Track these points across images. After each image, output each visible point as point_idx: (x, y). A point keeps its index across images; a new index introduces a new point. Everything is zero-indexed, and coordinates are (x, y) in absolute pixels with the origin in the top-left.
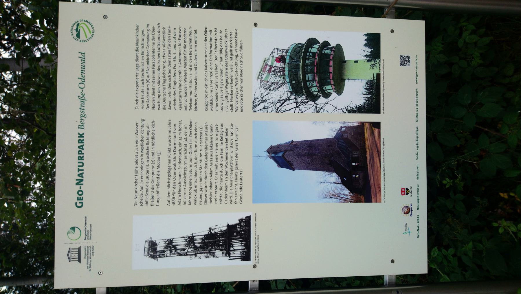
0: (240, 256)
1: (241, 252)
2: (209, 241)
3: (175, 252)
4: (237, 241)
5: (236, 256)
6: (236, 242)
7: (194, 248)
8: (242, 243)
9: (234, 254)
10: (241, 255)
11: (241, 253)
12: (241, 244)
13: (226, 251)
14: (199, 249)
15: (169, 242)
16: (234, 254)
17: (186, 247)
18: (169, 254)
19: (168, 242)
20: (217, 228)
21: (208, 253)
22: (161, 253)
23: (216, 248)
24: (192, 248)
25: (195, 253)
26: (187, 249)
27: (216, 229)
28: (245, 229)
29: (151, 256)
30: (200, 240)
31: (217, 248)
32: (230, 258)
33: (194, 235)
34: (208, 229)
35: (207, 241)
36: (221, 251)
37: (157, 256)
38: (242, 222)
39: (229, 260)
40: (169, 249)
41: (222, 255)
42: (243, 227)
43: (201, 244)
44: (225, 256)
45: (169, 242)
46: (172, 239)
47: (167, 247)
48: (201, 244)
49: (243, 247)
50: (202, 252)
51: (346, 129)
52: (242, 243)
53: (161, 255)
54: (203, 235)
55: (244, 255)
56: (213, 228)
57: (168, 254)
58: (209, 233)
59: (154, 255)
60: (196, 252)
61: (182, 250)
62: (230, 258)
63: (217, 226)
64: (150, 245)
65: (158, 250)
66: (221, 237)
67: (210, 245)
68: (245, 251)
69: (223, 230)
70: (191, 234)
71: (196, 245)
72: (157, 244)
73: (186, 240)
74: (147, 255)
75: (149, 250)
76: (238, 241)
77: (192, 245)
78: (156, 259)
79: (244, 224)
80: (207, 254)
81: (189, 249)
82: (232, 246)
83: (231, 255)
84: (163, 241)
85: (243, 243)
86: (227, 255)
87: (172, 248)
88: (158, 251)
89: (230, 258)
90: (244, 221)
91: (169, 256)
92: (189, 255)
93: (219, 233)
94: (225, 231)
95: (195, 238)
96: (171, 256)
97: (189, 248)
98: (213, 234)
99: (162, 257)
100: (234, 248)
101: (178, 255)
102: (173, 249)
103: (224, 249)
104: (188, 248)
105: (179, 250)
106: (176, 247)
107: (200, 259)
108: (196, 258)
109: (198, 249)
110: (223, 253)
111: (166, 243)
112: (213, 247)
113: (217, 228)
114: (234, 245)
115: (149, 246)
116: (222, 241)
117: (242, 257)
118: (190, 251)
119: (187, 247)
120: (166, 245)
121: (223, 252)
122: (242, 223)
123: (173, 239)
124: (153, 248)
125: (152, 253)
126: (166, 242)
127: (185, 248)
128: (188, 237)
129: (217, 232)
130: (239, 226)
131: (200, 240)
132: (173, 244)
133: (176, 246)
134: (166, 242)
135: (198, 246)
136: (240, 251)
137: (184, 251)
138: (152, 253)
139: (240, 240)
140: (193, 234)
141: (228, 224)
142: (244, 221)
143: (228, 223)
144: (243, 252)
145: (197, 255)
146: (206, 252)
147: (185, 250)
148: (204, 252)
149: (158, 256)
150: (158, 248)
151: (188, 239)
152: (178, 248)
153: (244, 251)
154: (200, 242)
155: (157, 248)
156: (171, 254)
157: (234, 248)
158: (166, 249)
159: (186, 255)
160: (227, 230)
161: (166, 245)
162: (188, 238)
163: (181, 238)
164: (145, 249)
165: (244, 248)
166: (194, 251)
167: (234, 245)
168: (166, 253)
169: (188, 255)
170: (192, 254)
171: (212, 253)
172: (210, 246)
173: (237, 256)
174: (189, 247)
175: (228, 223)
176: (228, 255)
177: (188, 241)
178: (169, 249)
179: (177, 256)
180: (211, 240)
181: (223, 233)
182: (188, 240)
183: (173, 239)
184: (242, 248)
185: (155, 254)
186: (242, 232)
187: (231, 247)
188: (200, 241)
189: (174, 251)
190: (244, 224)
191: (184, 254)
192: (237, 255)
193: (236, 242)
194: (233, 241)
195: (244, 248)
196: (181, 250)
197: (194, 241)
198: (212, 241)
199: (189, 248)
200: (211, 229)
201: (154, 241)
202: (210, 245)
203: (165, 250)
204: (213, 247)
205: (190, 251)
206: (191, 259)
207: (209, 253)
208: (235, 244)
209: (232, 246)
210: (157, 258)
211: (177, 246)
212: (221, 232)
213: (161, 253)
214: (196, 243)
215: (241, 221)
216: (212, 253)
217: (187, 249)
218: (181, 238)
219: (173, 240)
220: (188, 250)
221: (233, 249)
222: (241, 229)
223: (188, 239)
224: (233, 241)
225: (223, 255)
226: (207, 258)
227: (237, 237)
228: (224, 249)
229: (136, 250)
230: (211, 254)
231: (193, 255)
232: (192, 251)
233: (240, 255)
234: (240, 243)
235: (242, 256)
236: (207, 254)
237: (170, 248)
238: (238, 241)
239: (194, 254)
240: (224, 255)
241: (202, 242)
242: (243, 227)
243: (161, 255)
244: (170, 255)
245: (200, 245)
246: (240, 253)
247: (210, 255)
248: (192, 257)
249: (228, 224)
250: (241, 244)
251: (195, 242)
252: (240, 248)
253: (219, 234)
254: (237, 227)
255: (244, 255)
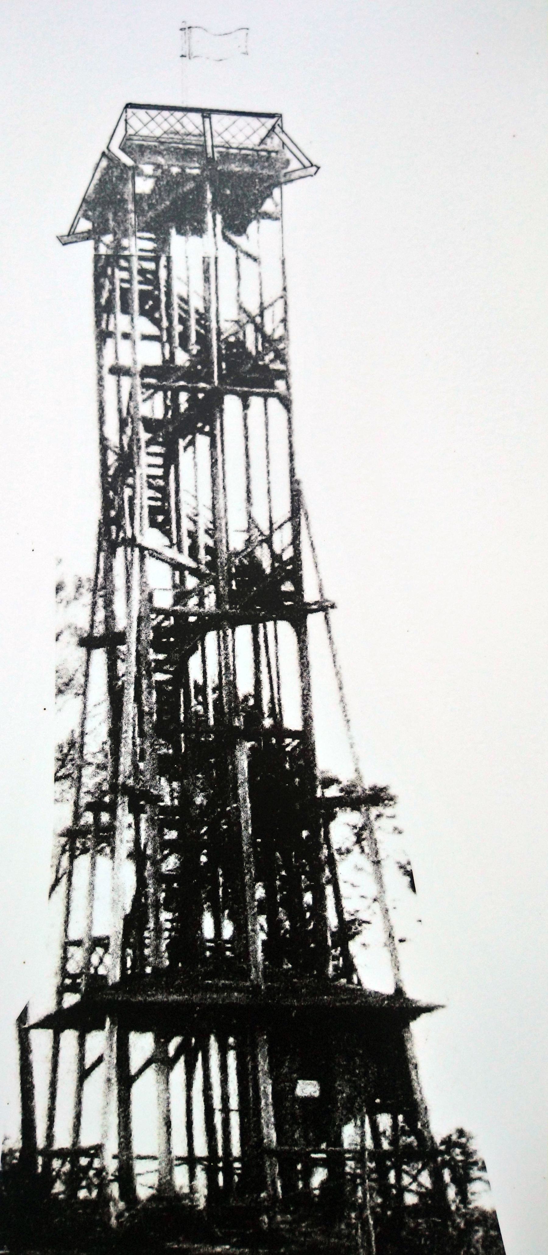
0: (50, 1137)
1: (97, 1150)
2: (243, 791)
3: (149, 424)
4: (226, 1110)
5: (53, 1096)
6: (217, 1103)
7: (181, 617)
8: (199, 1169)
9: (84, 1074)
10: (62, 1154)
11: (85, 1152)
12: (191, 1161)
13: (115, 976)
14: (159, 677)
15: (260, 356)
16: (84, 1074)
17: (186, 542)
18: (125, 361)
19: (250, 345)
20: (379, 879)
21: (116, 773)
22: (142, 272)
23: (156, 864)
24: (181, 596)
25: (121, 638)
26: (172, 553)
27: (369, 867)
28: (361, 1208)
29: (122, 179)
30: (258, 683)
31: (159, 877)
32: (37, 1026)
33: (314, 621)
34: (368, 783)
35: (243, 763)
36: (120, 925)
37: (108, 238)
38: (436, 1177)
39: (23, 1018)
40: (182, 359)
41: (74, 935)
42: (383, 1188)
43: (211, 697)
44: (64, 973)
45: (260, 356)
46: (280, 385)
47: (203, 340)
48: (211, 697)
49: (154, 1179)
50: (130, 709)
51: (353, 1235)
52: (199, 1169)
53: (120, 275)
54: (307, 720)
55: (59, 1187)
56: (378, 835)
57: (124, 346)
58: (328, 782)
59: (124, 201)
60: (132, 637)
61: (165, 497)
62: (42, 1024)
63: (410, 874)
64: (235, 167)
65: (176, 239)
66: (274, 925)
67: (199, 800)
68: (104, 1199)
69: (354, 946)
70: (330, 596)
71: (211, 638)
72: (241, 230)
73: (268, 541)
74: (127, 138)
75: (186, 154)
76: (218, 1118)
77: (210, 602)
78: (85, 225)
79: (410, 1199)
80: (102, 767)
81: (166, 569)
82: (172, 1048)
83: (69, 1037)
84: (272, 292)
85: (192, 1176)
86: (74, 988)
87: (193, 392)
88: (163, 242)
89: (37, 1026)
90: (451, 1192)
91: (109, 361)
92: (109, 569)
93: (319, 899)
94: (349, 968)
95: (285, 628)
96: (101, 379)
97: (177, 566)
98: (314, 834)
99: (98, 289)
100: (151, 1073)
101: (112, 459)
102: (175, 399)
103: (140, 960)
104: (185, 559)
105: (166, 466)
106: (195, 431)
107: (51, 684)
108: (70, 640)
109: (160, 667)
110: (102, 942)
111: (250, 329)
112: (172, 835)
113: (379, 879)
114: (179, 1070)
115: (226, 157)
116: (228, 929)
117: (47, 1165)
118: (143, 584)
119: (193, 552)
120: (228, 328)
121: (115, 943)
122: (425, 1179)
123: (286, 402)
124: (199, 190)
125: (144, 186)
126: (259, 329)
127: (186, 525)
128: (296, 559)
129: (334, 881)
130: (394, 1142)
131: (258, 683)
132: (232, 403)
133: (212, 435)
134: (259, 329)
135: (194, 662)
136: (112, 1147)
137: (153, 511)
138: (144, 186)
139: (236, 1150)
140: (324, 607)
141: (417, 1011)
142: (451, 1192)
143: (429, 1009)
144: (100, 1171)
145: (100, 656)
146: (126, 749)
147: (164, 528)
148: (129, 731)
149: (118, 247)
150: (194, 240)
151: (275, 557)
152: (185, 458)
153: (103, 1186)
154: (233, 685)
155: (199, 231)
156: (126, 381)
157: (151, 1073)
158: (178, 328)
159: (104, 533)
160: (359, 992)
161: (228, 328)
162: (288, 555)
163: (294, 482)
164: (196, 118)
165: (143, 1192)
166: (140, 619)
167: (179, 1070)
168: (145, 326)
169: (112, 553)
170: (108, 604)
171: (105, 817)
172: (186, 797)
173: (52, 1109)
174: (195, 572)
175: (429, 1009)
176: (71, 999)
177: (251, 555)
178: (182, 359)
179: (103, 439)
180: (246, 814)
181: (323, 954)
182: (263, 555)
183: (286, 402)
184: (139, 1167)
185: (139, 212)
186: (319, 1176)
187: (161, 1043)
188: (245, 687)
189: (159, 414)
190: (410, 1199)
191: (118, 521)
192: (184, 1119)
193: (217, 1103)
194: (224, 1068)
195: (143, 1192)
196: (163, 490)
197: (255, 622)
198: (235, 823)
199: (177, 566)
200: (374, 811)
201: (268, 206)
202: (199, 800)
203: (176, 313)
204: (172, 835)
205: (143, 584)
206: (59, 588)
207: (115, 788)
208: (189, 1086)
209: (172, 1048)
210: (87, 236)
211: (203, 441)
212: (333, 921)
213: (142, 272)
214: (222, 641)
215: (452, 1165)
216: (105, 817)
217: (172, 553)
218: (294, 482)
219: (273, 402)
220: (156, 555)
221: (135, 1063)
222: (359, 1155)
223: (275, 557)
224: (224, 1068)
225: (78, 943)
226: (63, 761)
227: (268, 1114)
228: (140, 960)
229: (186, 29)
230: (96, 807)
231: (101, 615)
232: (151, 596)
233: (63, 1140)
234: (201, 1149)
235: (56, 1163)
236: (102, 767)
237: (190, 374)
238: (218, 1118)
239: (110, 617)
240: (77, 956)
241: (235, 712)
242: (383, 1188)
243: (120, 275)
244: (117, 371)
245: (201, 690)
246: (86, 1142)
247: (86, 799)
248: (87, 597)
249: (417, 1011)
250: (191, 1161)
251: (244, 632)
252: (137, 1148)
253: (308, 898)
254: (382, 1109)
255: (59, 1187)
